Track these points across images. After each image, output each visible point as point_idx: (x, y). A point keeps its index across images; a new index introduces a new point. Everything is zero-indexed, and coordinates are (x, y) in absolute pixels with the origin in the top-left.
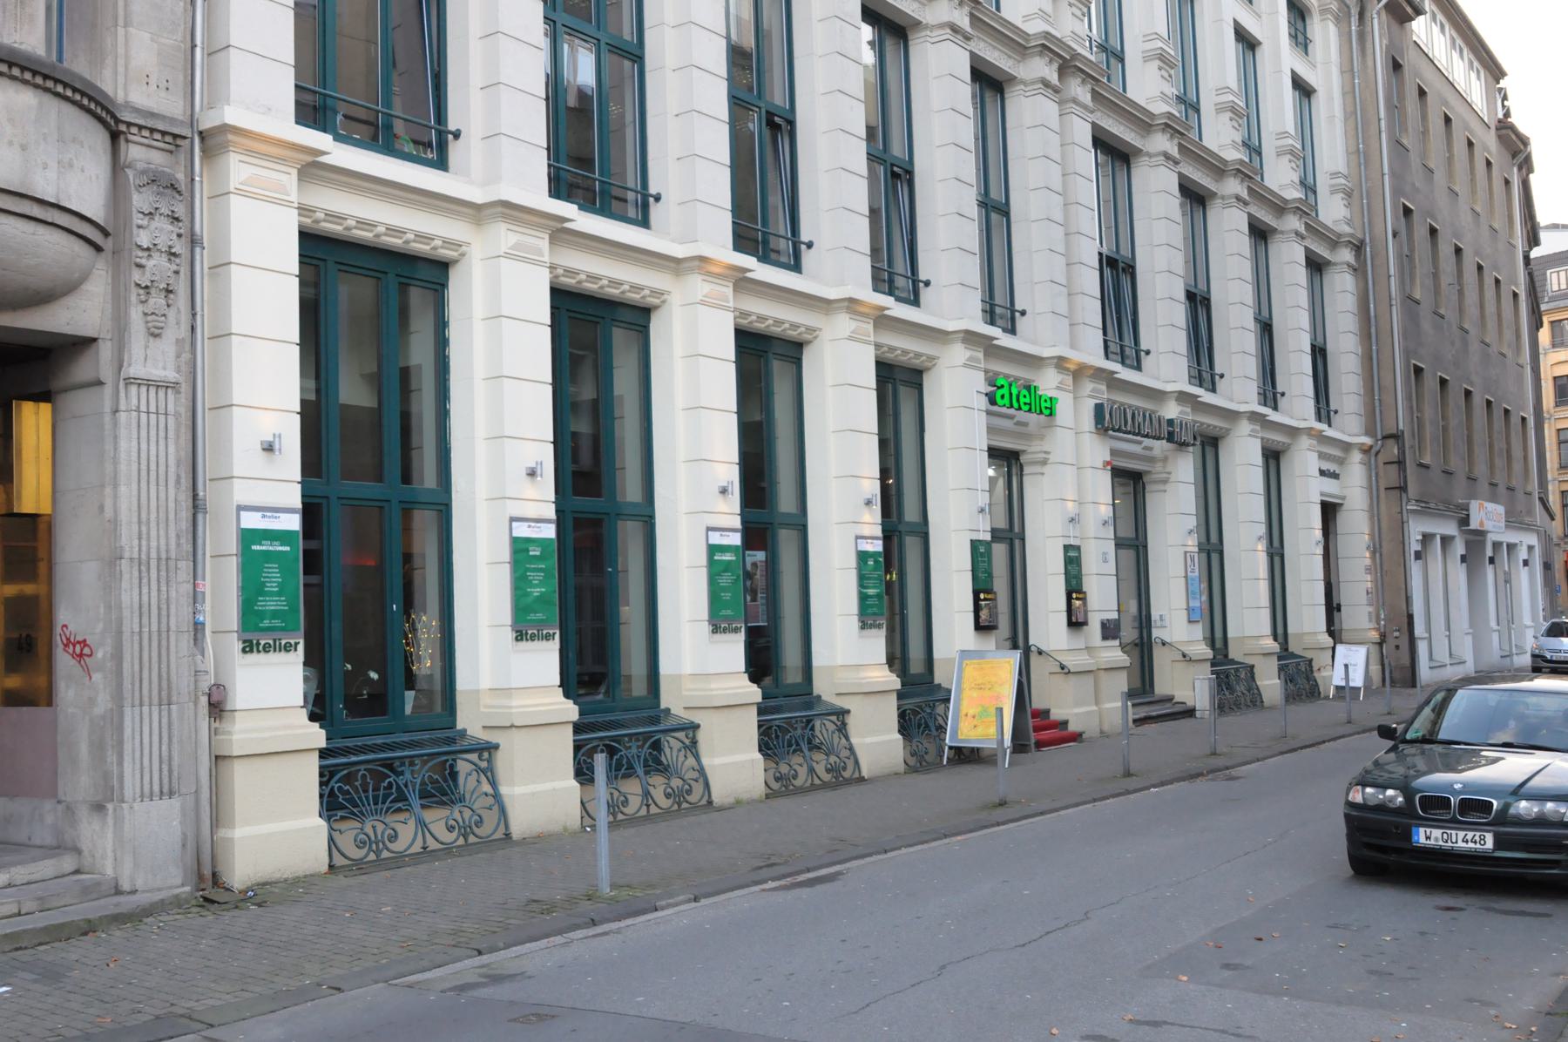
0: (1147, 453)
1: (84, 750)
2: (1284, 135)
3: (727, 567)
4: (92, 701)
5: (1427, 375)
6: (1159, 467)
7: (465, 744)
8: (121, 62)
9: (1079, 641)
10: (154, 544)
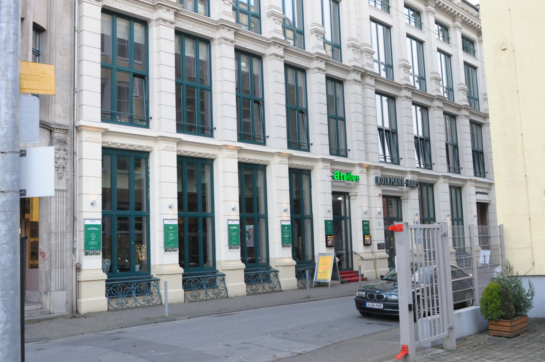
1: (44, 278)
2: (461, 84)
4: (45, 267)
6: (405, 194)
9: (369, 250)
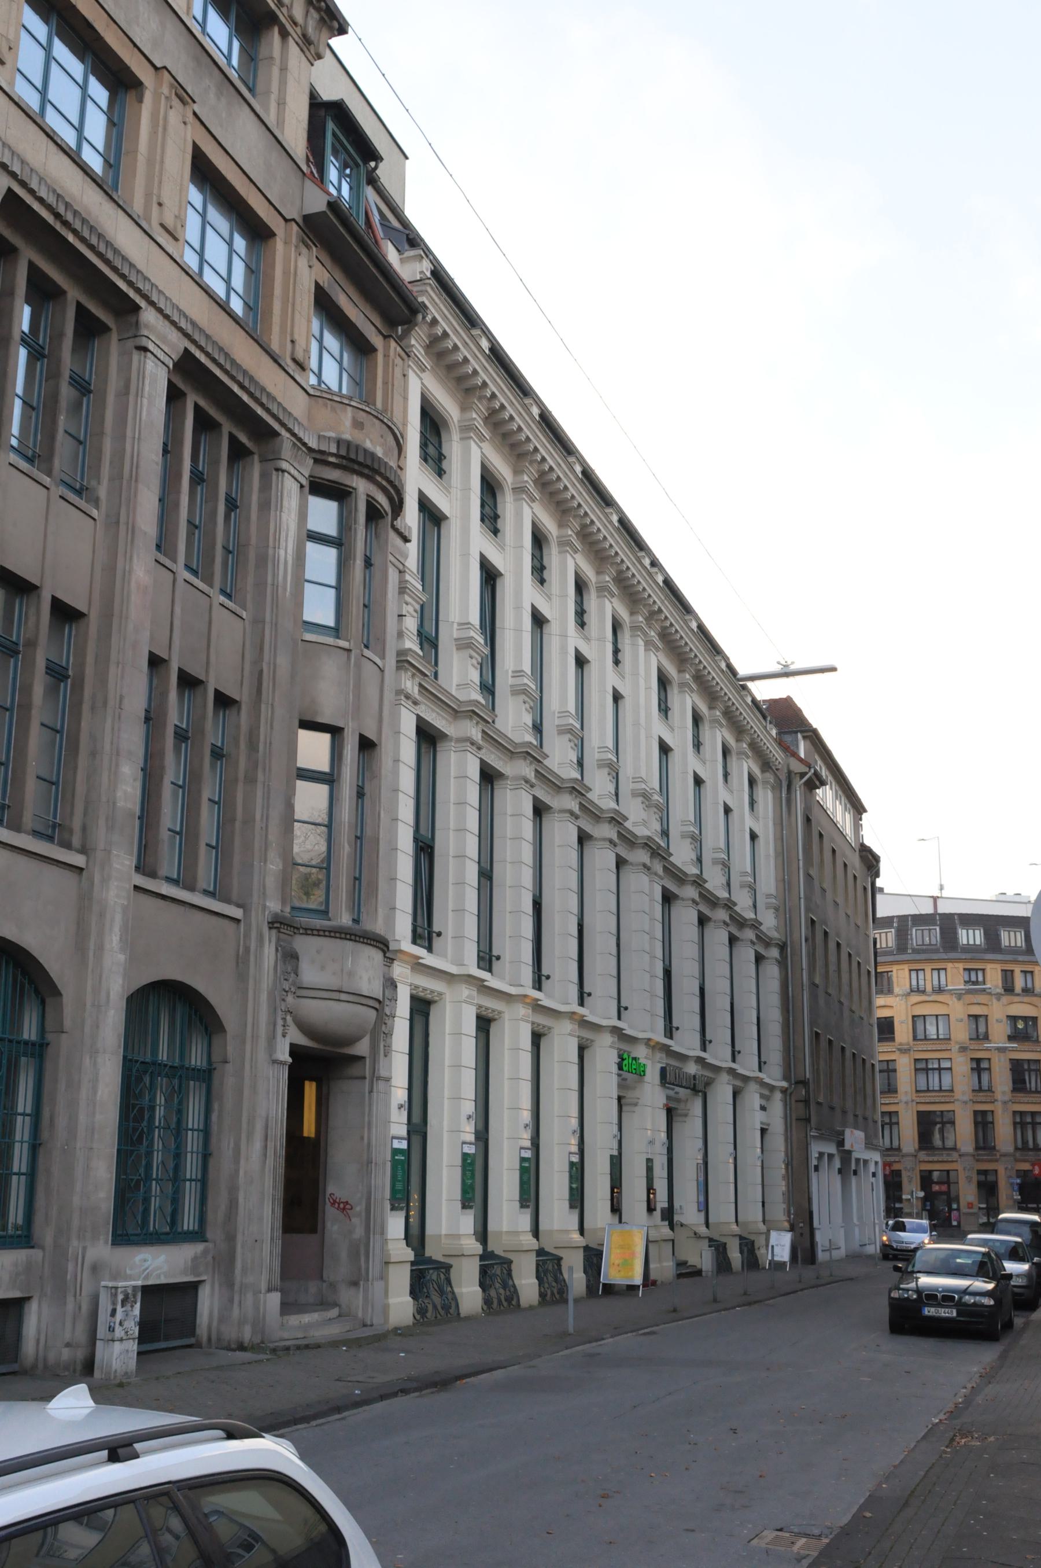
0: (677, 1096)
5: (822, 1038)
6: (682, 1106)
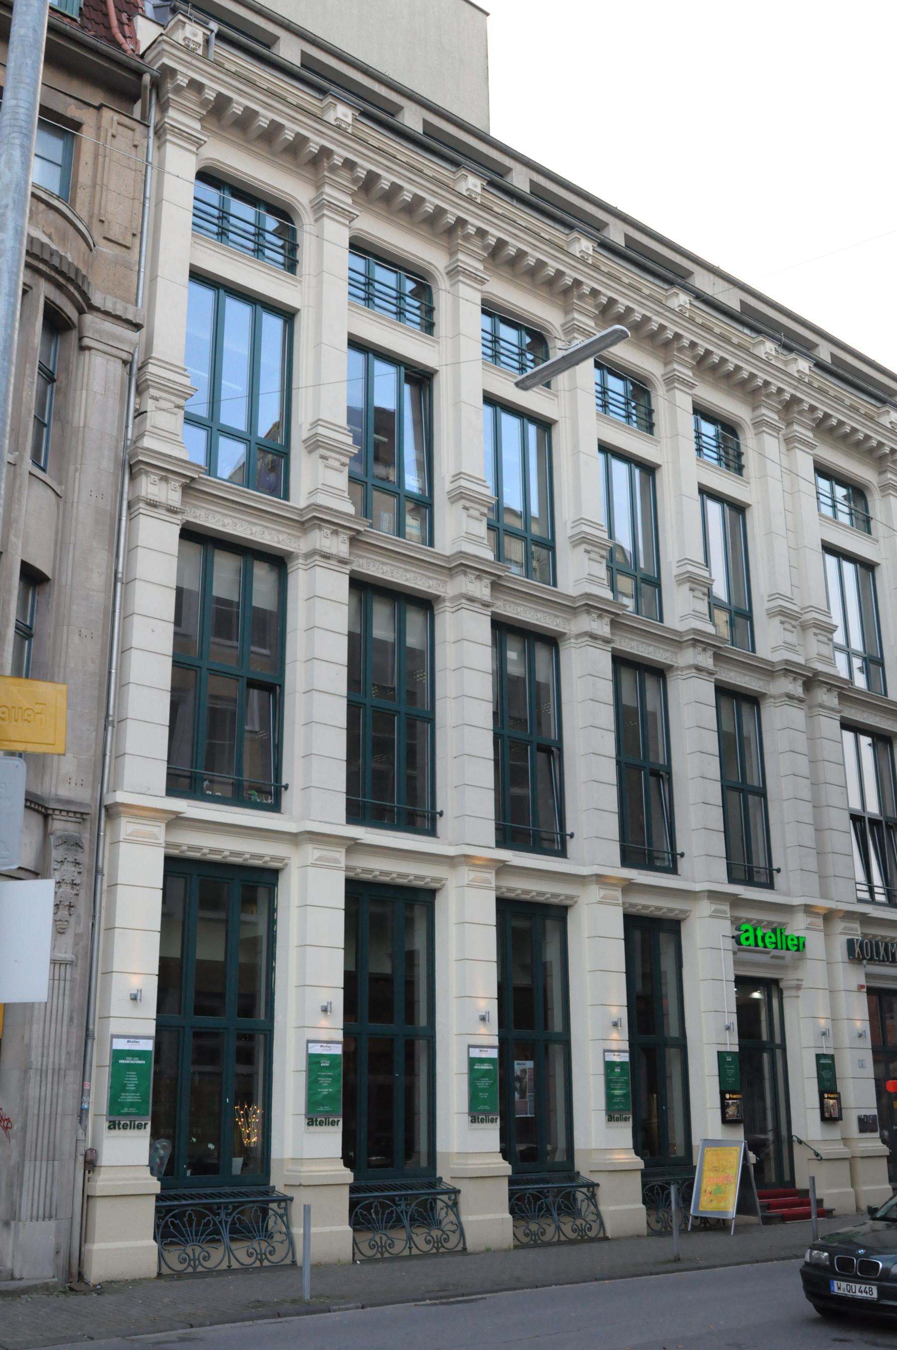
3: (486, 1073)
7: (580, 1182)
8: (55, 772)
9: (835, 1133)
10: (51, 1060)
